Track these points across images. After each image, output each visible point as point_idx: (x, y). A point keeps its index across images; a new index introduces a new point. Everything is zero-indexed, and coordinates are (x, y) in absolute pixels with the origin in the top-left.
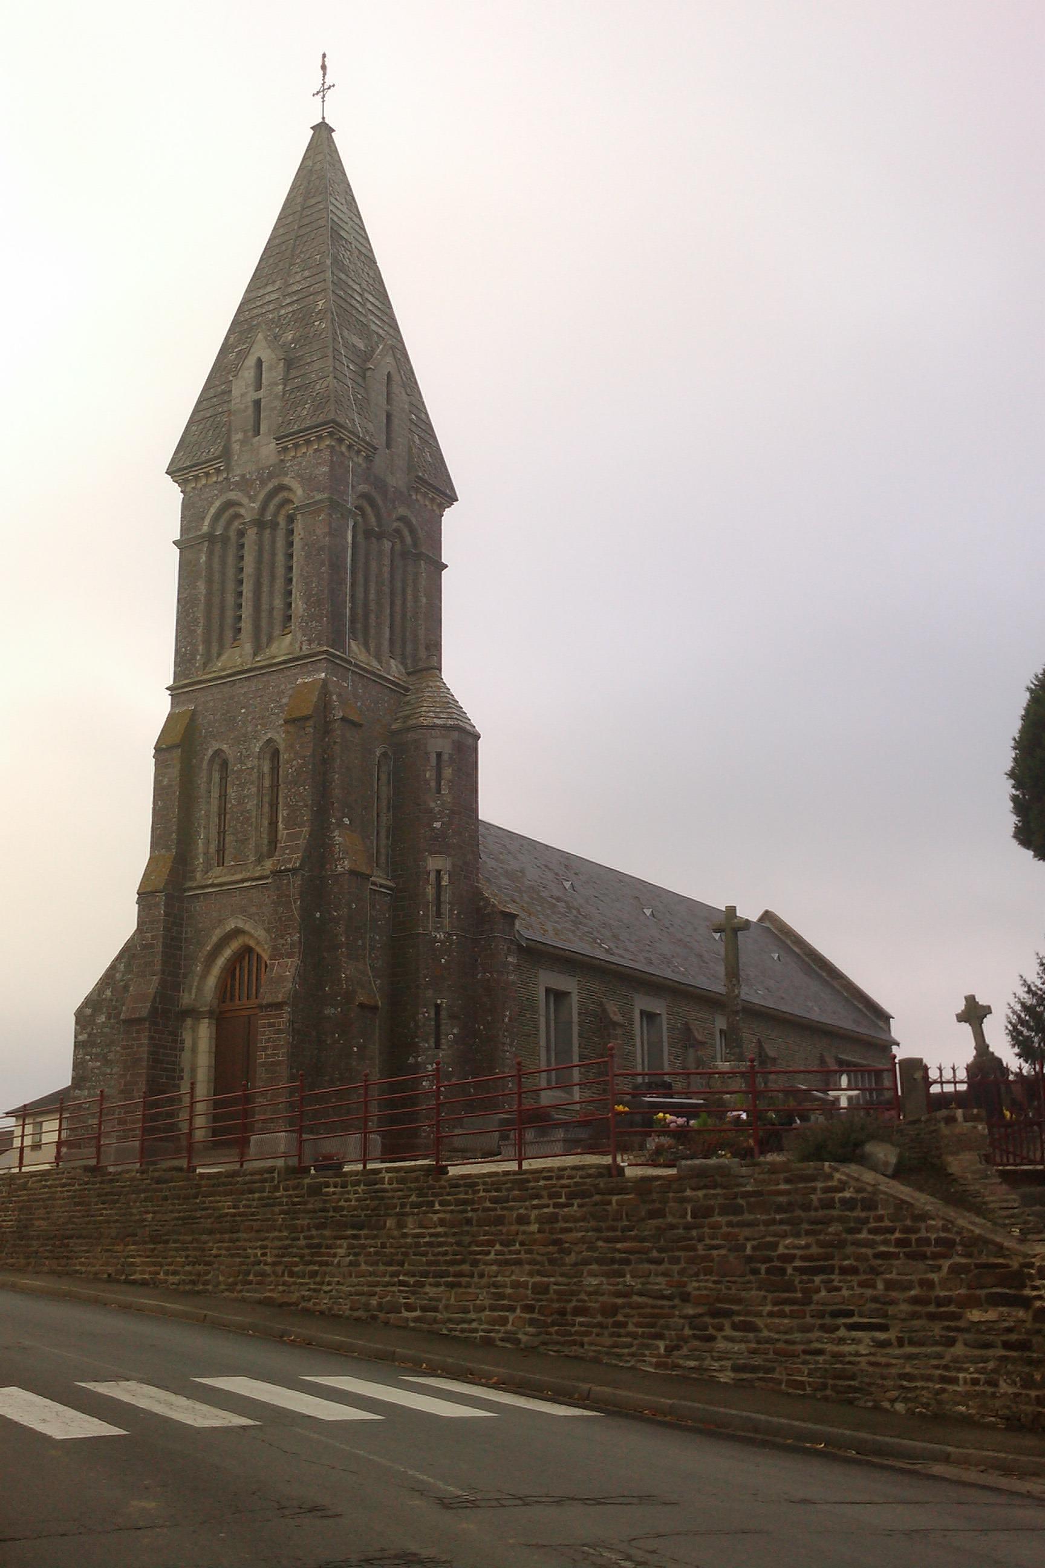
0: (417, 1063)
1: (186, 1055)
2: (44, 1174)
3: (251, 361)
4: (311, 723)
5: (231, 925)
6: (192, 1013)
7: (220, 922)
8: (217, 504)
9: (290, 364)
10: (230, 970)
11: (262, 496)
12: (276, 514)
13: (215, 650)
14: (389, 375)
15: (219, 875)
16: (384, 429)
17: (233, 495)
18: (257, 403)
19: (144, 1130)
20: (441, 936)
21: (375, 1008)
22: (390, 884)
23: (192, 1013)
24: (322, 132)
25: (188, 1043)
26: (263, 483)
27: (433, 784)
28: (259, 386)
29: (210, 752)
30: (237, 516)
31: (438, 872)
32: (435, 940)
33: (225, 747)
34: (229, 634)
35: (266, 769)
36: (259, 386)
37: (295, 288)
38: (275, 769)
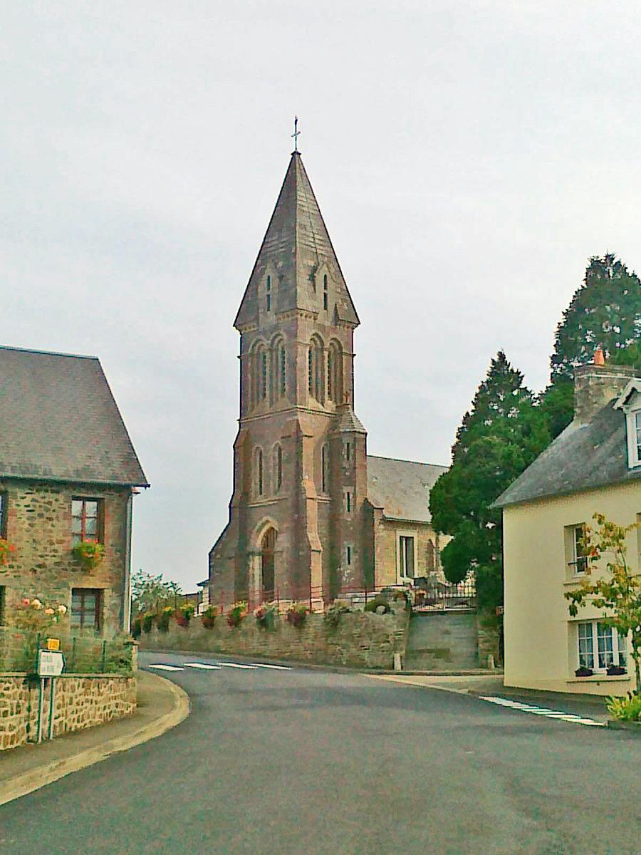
0: (340, 571)
1: (251, 570)
2: (433, 518)
3: (265, 277)
4: (233, 560)
5: (265, 519)
6: (253, 553)
7: (261, 519)
8: (255, 340)
9: (281, 278)
10: (267, 537)
11: (271, 338)
12: (278, 345)
13: (256, 403)
14: (325, 276)
15: (261, 500)
16: (283, 409)
17: (259, 337)
18: (268, 296)
19: (248, 594)
20: (349, 519)
21: (320, 551)
22: (328, 498)
23: (253, 553)
24: (295, 154)
25: (251, 566)
26: (272, 333)
27: (346, 456)
28: (269, 289)
29: (255, 448)
30: (262, 345)
31: (348, 493)
32: (347, 521)
33: (260, 446)
34: (261, 396)
35: (277, 455)
36: (269, 289)
37: (285, 240)
38: (280, 455)
